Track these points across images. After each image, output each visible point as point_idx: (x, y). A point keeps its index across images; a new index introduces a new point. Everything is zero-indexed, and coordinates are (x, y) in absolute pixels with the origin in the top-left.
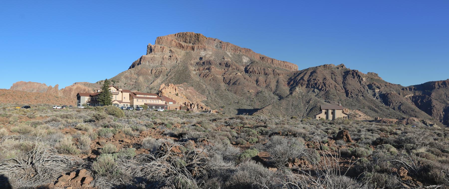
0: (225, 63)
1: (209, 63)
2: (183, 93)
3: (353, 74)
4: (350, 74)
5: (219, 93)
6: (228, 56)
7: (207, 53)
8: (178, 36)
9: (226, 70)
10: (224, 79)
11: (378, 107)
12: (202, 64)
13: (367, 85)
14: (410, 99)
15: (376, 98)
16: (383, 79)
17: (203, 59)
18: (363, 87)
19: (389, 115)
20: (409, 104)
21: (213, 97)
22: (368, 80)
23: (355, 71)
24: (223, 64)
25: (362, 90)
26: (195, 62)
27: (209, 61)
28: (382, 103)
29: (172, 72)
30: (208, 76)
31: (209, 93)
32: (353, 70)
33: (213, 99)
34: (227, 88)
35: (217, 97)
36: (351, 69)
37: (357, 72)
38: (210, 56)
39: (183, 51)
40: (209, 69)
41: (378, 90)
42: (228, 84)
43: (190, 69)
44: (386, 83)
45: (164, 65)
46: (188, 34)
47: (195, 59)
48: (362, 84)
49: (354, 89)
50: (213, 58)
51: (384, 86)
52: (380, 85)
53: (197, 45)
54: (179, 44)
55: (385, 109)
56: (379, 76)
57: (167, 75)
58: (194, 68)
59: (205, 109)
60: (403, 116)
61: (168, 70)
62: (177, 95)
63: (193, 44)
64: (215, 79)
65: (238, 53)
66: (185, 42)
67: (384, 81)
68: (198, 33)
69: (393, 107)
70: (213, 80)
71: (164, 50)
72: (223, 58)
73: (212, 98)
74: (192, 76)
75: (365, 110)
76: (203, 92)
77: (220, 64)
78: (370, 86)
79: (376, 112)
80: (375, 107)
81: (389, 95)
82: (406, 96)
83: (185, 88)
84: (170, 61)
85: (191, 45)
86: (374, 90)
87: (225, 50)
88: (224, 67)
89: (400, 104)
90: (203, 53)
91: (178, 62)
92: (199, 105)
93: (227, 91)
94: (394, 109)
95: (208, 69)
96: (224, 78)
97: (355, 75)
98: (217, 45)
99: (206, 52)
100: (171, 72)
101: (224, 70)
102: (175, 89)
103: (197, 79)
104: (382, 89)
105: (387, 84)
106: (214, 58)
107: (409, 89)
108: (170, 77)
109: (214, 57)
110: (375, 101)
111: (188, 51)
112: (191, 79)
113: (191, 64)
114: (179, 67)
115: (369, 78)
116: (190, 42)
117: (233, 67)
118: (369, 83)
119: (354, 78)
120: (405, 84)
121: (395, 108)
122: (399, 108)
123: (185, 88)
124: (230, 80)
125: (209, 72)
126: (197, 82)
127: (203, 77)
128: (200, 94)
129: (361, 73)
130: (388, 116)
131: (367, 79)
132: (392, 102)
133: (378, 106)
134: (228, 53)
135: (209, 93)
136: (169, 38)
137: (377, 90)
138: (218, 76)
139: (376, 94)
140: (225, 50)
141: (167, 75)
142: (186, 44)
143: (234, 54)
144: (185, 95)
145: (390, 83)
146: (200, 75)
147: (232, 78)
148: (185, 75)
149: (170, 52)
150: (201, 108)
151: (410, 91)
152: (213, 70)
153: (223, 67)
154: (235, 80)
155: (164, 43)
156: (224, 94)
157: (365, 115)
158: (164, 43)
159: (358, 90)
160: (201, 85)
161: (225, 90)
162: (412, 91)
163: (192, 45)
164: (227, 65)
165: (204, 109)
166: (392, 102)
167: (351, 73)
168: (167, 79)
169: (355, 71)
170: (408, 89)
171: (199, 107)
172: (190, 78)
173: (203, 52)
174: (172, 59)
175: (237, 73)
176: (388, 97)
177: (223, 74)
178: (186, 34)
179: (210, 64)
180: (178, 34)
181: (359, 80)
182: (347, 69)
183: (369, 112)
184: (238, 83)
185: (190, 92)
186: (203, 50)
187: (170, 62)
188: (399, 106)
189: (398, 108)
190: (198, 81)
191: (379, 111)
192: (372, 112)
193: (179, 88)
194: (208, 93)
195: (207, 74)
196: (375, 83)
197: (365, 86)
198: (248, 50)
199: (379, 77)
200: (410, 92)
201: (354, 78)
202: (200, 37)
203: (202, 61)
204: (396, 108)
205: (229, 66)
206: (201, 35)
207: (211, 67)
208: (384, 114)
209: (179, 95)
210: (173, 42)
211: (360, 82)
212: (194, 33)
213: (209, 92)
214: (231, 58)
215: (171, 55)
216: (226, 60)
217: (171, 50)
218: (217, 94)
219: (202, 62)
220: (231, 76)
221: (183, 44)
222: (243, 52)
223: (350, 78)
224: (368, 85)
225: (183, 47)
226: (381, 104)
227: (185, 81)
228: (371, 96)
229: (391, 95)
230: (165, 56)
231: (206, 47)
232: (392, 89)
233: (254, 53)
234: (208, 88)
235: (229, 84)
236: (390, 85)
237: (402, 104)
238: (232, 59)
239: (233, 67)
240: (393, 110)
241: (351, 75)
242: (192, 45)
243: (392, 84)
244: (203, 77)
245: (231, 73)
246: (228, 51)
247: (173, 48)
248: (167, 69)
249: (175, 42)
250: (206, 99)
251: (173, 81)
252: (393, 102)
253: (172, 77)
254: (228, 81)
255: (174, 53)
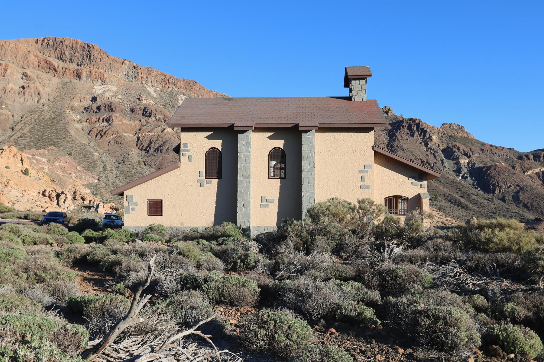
0: (143, 108)
1: (110, 108)
2: (43, 168)
3: (410, 128)
4: (403, 127)
5: (125, 169)
6: (149, 94)
7: (107, 88)
8: (44, 44)
9: (143, 122)
10: (137, 142)
11: (467, 196)
12: (95, 110)
13: (442, 151)
14: (539, 177)
15: (463, 177)
16: (476, 138)
17: (98, 99)
18: (434, 154)
19: (494, 213)
20: (537, 189)
21: (112, 177)
22: (444, 139)
23: (414, 121)
24: (137, 109)
25: (431, 159)
26: (82, 106)
27: (108, 103)
28: (477, 188)
29: (25, 123)
30: (105, 133)
31: (105, 170)
32: (411, 120)
33: (111, 181)
34: (144, 160)
35: (121, 178)
36: (407, 116)
37: (419, 124)
38: (112, 94)
39: (56, 78)
40: (109, 120)
41: (467, 161)
42: (145, 150)
43: (69, 117)
44: (484, 144)
45: (7, 105)
46: (67, 42)
47: (82, 100)
48: (430, 148)
49: (413, 158)
50: (118, 98)
51: (479, 151)
52: (471, 149)
53: (88, 68)
54: (46, 61)
55: (482, 201)
56: (467, 130)
57: (13, 129)
58: (78, 116)
59: (90, 201)
60: (526, 215)
61: (17, 118)
62: (26, 172)
63: (78, 65)
64: (119, 141)
65: (171, 89)
66: (61, 59)
67: (478, 142)
68: (90, 44)
69: (500, 197)
70: (116, 142)
71: (9, 71)
72: (139, 99)
73: (108, 180)
74: (72, 132)
75: (438, 203)
76: (91, 166)
77: (132, 110)
78: (448, 153)
79: (463, 208)
80: (461, 197)
81: (492, 170)
82: (530, 172)
83: (51, 158)
84: (22, 99)
85: (74, 66)
86: (456, 160)
87: (144, 82)
88: (140, 116)
89: (518, 188)
90: (98, 89)
91: (41, 101)
92: (78, 193)
93: (143, 166)
94: (503, 200)
95: (107, 120)
96: (138, 139)
97: (415, 129)
98: (128, 72)
99: (104, 86)
100: (22, 122)
101: (138, 121)
102: (22, 160)
103: (84, 140)
104: (475, 157)
105: (483, 148)
106: (121, 99)
107: (534, 157)
108: (19, 134)
109: (120, 97)
110: (460, 183)
111: (66, 80)
112: (68, 139)
113: (72, 108)
114: (44, 113)
115: (444, 136)
116: (71, 61)
117: (158, 116)
118: (445, 147)
119: (412, 135)
120: (525, 148)
121: (506, 198)
122: (516, 198)
123: (51, 158)
124: (151, 143)
125: (109, 127)
126: (83, 147)
127: (97, 135)
128: (85, 171)
129: (427, 124)
130: (491, 216)
131: (440, 139)
132: (498, 186)
133: (468, 195)
134: (149, 89)
135: (105, 170)
136: (20, 45)
137: (464, 161)
138: (126, 134)
139: (461, 168)
140: (144, 82)
141: (13, 129)
142: (62, 64)
143: (161, 91)
144: (47, 174)
145: (491, 146)
146: (90, 131)
147: (155, 139)
148: (56, 129)
149: (24, 77)
150: (81, 200)
151: (536, 160)
152: (116, 122)
153: (138, 117)
154: (160, 144)
155: (9, 55)
156: (135, 170)
157: (441, 213)
158: (9, 55)
159: (422, 162)
160: (90, 152)
161: (139, 162)
162: (539, 161)
163: (76, 67)
164: (146, 112)
165: (87, 202)
166: (498, 186)
167: (407, 125)
168: (12, 139)
169: (414, 121)
170: (531, 157)
171: (78, 197)
172: (67, 137)
173: (99, 87)
174: (27, 93)
175: (164, 129)
176: (489, 174)
177: (137, 131)
178: (61, 42)
179: (112, 110)
180: (44, 39)
181: (424, 138)
182: (396, 116)
183: (447, 207)
184: (166, 149)
185: (62, 168)
186: (99, 82)
187: (22, 99)
188: (515, 193)
189: (513, 197)
190: (85, 146)
191: (471, 205)
192: (455, 208)
193: (37, 157)
194: (101, 169)
195: (104, 131)
196: (458, 145)
197: (436, 152)
198: (192, 83)
199: (467, 133)
200: (536, 163)
201: (412, 135)
202: (95, 51)
203: (95, 104)
204: (509, 197)
205: (150, 113)
206: (96, 47)
207: (113, 115)
208: (483, 211)
209: (32, 172)
210: (32, 57)
211: (426, 144)
212: (80, 41)
213: (104, 167)
214: (155, 99)
215: (26, 85)
216: (144, 102)
217: (25, 74)
218: (121, 171)
219: (95, 106)
220: (153, 134)
221: (56, 63)
222: (181, 87)
223: (404, 136)
224: (443, 151)
225: (55, 70)
226: (474, 191)
227: (54, 144)
228: (451, 172)
229: (495, 169)
230: (10, 86)
231: (105, 76)
232: (496, 158)
233: (203, 88)
234: (103, 158)
235: (147, 150)
236: (491, 150)
237: (522, 189)
238: (157, 100)
239: (158, 116)
240: (503, 203)
241: (407, 130)
242: (76, 67)
243: (496, 147)
244: (97, 135)
245: (153, 129)
246: (150, 84)
247: (31, 69)
248: (13, 116)
249: (36, 56)
250: (96, 181)
251: (25, 142)
252: (501, 184)
253: (25, 134)
254: (146, 145)
255: (33, 81)
